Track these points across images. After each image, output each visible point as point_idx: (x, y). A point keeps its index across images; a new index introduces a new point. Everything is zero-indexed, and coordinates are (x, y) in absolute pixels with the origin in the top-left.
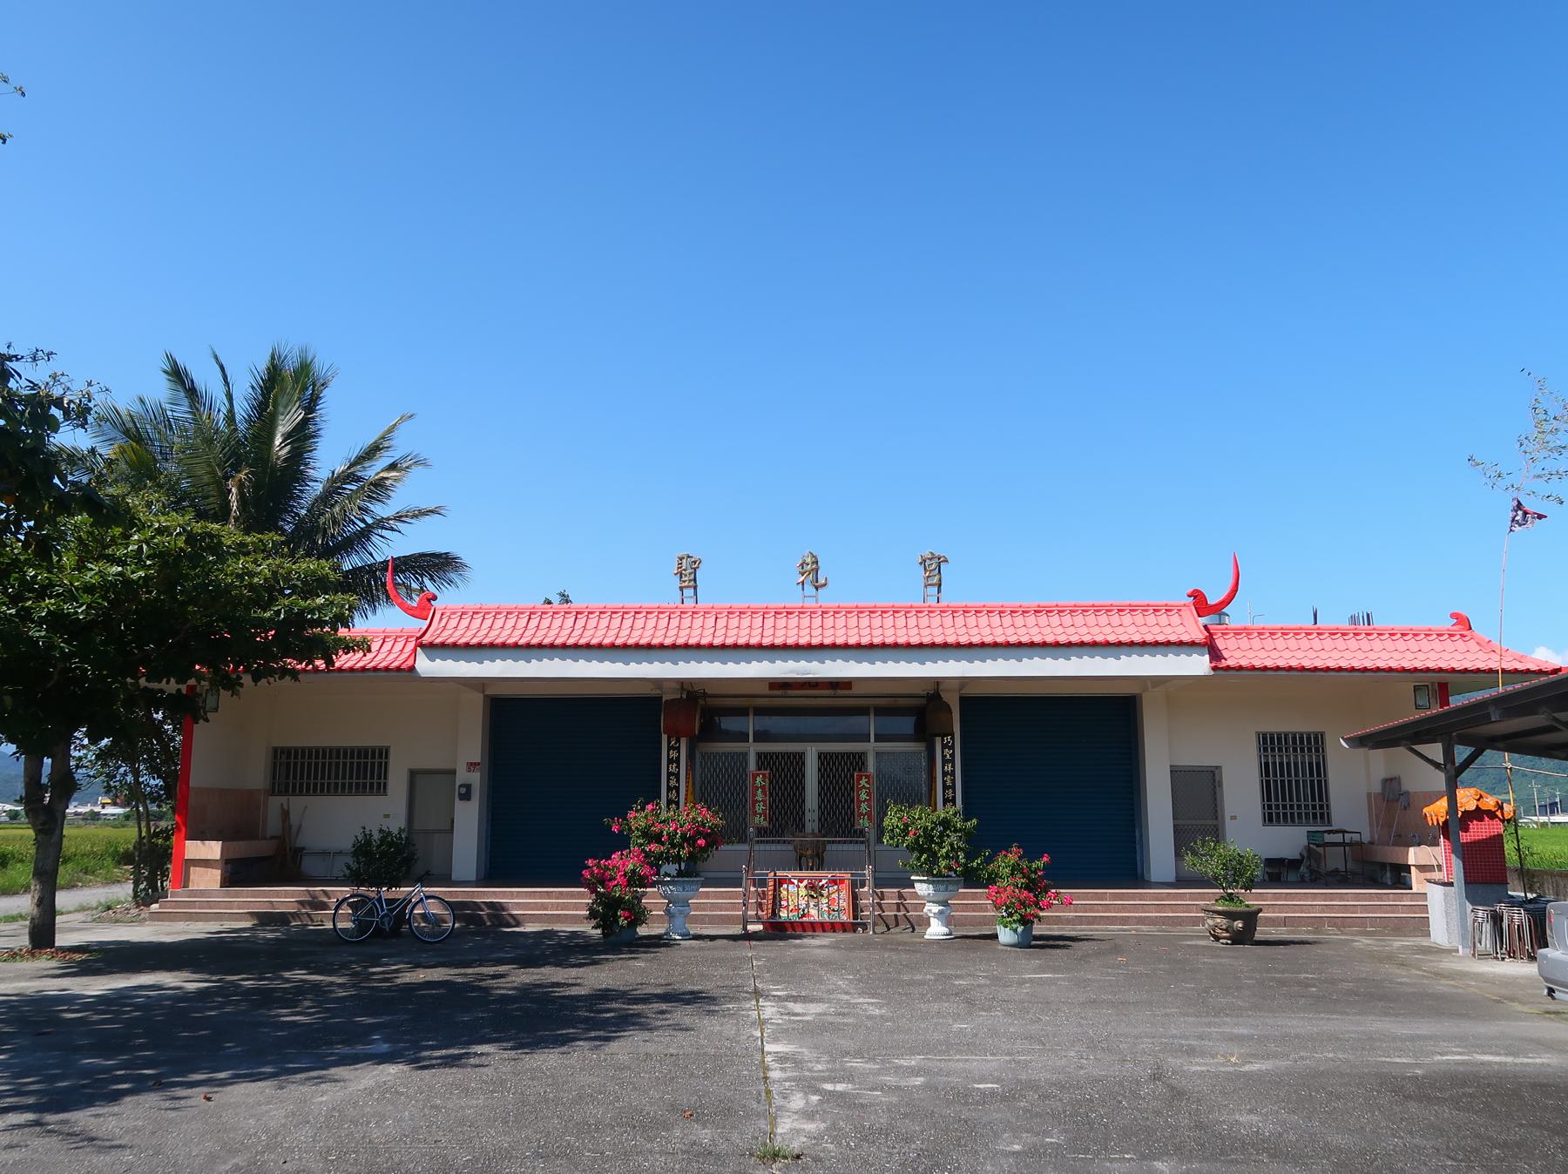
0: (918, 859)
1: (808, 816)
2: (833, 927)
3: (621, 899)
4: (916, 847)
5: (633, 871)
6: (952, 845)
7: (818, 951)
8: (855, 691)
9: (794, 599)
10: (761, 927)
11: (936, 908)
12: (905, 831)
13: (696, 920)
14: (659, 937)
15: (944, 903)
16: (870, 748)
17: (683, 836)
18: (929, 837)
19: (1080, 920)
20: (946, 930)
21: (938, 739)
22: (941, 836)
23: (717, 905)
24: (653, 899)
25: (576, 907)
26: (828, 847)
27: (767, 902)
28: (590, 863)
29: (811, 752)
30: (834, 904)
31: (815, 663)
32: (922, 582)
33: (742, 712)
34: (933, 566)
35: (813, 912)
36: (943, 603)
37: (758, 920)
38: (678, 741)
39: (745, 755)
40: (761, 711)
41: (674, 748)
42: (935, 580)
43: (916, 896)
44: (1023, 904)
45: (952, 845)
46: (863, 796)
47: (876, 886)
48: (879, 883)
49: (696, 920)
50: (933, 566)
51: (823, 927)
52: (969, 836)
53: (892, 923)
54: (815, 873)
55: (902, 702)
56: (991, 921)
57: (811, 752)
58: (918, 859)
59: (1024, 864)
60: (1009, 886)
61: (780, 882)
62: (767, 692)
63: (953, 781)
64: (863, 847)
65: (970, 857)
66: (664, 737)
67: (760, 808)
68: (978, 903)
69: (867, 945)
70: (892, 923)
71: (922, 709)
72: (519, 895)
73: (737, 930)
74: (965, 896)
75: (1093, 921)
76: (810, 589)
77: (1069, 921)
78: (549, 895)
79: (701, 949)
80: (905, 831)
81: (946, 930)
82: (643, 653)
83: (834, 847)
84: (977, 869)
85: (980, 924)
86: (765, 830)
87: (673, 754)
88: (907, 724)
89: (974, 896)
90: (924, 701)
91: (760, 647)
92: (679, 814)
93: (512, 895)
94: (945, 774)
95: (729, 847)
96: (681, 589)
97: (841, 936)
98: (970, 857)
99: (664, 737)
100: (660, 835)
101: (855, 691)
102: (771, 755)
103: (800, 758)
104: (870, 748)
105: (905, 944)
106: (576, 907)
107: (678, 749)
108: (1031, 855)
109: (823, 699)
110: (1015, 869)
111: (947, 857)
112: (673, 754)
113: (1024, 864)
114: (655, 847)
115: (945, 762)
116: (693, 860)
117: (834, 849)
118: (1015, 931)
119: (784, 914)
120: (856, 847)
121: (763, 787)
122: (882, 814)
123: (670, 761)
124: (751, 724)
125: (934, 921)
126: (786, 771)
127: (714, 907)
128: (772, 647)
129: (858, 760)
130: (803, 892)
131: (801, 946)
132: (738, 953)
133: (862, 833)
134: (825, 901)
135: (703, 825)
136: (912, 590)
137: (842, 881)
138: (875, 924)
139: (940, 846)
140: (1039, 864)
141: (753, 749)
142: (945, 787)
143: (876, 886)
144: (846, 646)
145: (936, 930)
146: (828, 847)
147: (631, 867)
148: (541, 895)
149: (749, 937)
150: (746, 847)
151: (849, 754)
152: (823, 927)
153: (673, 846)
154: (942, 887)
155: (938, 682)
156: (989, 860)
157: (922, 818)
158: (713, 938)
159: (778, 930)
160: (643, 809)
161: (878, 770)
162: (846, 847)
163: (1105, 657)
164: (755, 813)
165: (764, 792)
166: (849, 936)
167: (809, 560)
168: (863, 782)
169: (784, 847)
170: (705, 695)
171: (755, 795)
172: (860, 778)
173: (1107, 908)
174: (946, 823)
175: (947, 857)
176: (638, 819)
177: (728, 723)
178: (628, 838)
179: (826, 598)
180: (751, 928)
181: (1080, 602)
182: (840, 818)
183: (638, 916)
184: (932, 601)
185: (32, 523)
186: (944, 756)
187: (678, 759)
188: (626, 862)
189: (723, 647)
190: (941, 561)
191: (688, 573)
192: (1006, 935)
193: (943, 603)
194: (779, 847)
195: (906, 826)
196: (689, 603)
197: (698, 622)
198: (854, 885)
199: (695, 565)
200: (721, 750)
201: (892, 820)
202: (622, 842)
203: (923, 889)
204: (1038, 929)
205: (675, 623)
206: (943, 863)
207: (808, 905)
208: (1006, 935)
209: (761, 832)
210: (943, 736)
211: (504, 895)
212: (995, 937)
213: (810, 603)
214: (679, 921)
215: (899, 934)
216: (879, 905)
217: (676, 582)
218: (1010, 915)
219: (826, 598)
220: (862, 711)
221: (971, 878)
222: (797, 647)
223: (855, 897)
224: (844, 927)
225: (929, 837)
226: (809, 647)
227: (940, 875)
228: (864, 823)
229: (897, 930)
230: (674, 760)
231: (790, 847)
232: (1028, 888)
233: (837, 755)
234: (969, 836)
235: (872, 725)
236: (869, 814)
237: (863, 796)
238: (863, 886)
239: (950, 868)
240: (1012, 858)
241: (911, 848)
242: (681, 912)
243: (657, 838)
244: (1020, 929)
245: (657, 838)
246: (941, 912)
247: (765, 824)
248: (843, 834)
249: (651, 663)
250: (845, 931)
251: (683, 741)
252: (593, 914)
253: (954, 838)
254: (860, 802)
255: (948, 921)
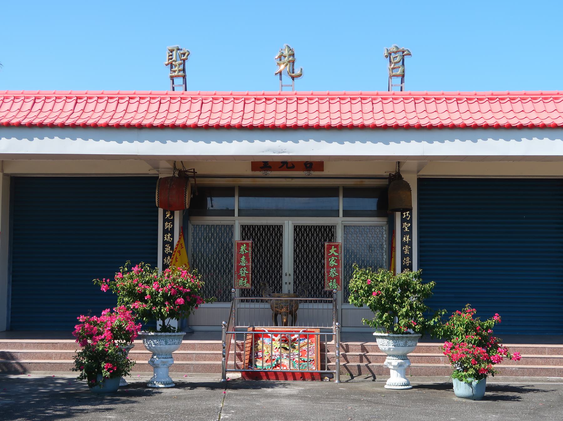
0: (381, 317)
1: (285, 279)
2: (303, 376)
3: (104, 352)
4: (378, 307)
5: (120, 327)
6: (411, 305)
7: (286, 402)
8: (328, 171)
9: (272, 87)
10: (239, 375)
11: (395, 362)
12: (369, 292)
13: (181, 368)
14: (144, 385)
15: (404, 357)
16: (339, 222)
17: (164, 296)
18: (390, 297)
19: (523, 372)
20: (404, 381)
21: (398, 214)
22: (402, 297)
23: (199, 357)
24: (139, 352)
25: (66, 356)
26: (301, 306)
27: (246, 354)
28: (81, 319)
29: (288, 226)
30: (304, 357)
31: (290, 143)
32: (387, 73)
33: (227, 192)
34: (398, 58)
35: (285, 362)
36: (406, 91)
37: (237, 368)
38: (172, 214)
39: (231, 227)
40: (246, 191)
41: (168, 220)
42: (399, 72)
43: (376, 348)
44: (477, 360)
45: (411, 305)
46: (333, 263)
47: (342, 339)
48: (344, 336)
49: (181, 368)
50: (398, 58)
51: (294, 376)
52: (426, 297)
53: (355, 372)
54: (288, 328)
55: (367, 182)
56: (446, 371)
57: (288, 226)
58: (381, 317)
59: (477, 323)
60: (466, 344)
61: (257, 337)
62: (249, 172)
63: (411, 250)
64: (331, 306)
65: (428, 316)
66: (161, 211)
67: (243, 272)
68: (434, 356)
69: (331, 396)
70: (355, 372)
71: (383, 189)
72: (27, 346)
73: (217, 378)
74: (420, 349)
75: (535, 372)
76: (287, 79)
77: (512, 372)
78: (54, 346)
79: (178, 398)
80: (369, 292)
81: (404, 381)
82: (135, 132)
83: (306, 306)
84: (434, 327)
85: (434, 374)
86: (248, 290)
87: (168, 226)
88: (371, 204)
89: (428, 349)
90: (386, 182)
91: (240, 127)
92: (171, 274)
93: (21, 346)
94: (403, 244)
95: (209, 305)
96: (172, 78)
97: (309, 384)
98: (428, 316)
99: (161, 211)
100: (144, 294)
101: (328, 171)
102: (253, 227)
103: (279, 229)
104: (339, 222)
105: (367, 393)
106: (66, 356)
107: (173, 221)
108: (483, 315)
109: (298, 178)
110: (469, 328)
111: (407, 315)
112: (168, 226)
113: (477, 323)
114: (140, 306)
115: (403, 233)
116: (178, 314)
117: (306, 308)
118: (470, 384)
119: (259, 364)
120: (325, 306)
121: (246, 255)
122: (348, 276)
123: (165, 232)
124: (236, 202)
125: (393, 373)
126: (265, 241)
127: (199, 357)
128: (251, 128)
129: (328, 233)
130: (277, 344)
131: (271, 396)
132: (205, 404)
133: (330, 294)
134: (296, 352)
135: (184, 285)
136: (377, 79)
137: (312, 336)
138: (340, 373)
139: (401, 306)
140: (490, 322)
141: (238, 222)
142: (403, 256)
143: (342, 339)
144: (318, 128)
145: (395, 380)
146: (301, 306)
147: (116, 323)
148: (47, 346)
149: (227, 385)
150: (228, 305)
151: (320, 227)
152: (294, 376)
153: (155, 304)
154: (401, 343)
155: (399, 161)
156: (445, 319)
157: (385, 280)
158: (193, 386)
159: (254, 379)
160: (130, 271)
161: (346, 239)
162: (315, 306)
163: (553, 139)
164: (239, 277)
165: (247, 259)
166: (317, 384)
167: (286, 53)
168: (332, 251)
169: (262, 305)
170: (195, 176)
171: (239, 261)
172: (330, 247)
173: (546, 361)
174: (405, 286)
175: (407, 315)
176: (124, 280)
177: (217, 203)
178: (116, 296)
179: (301, 87)
180: (231, 376)
181: (529, 91)
182: (312, 283)
183: (120, 366)
184: (396, 90)
185: (383, 303)
186: (402, 229)
187: (172, 229)
188: (114, 318)
189: (207, 127)
190: (404, 54)
191: (178, 64)
192: (461, 388)
193: (406, 91)
194: (257, 305)
195: (370, 287)
196: (179, 90)
197: (186, 107)
198: (322, 338)
199: (184, 57)
200: (210, 223)
201: (356, 282)
202: (110, 301)
203: (384, 344)
204: (490, 381)
205: (164, 107)
206: (403, 322)
207: (281, 355)
208: (461, 388)
209: (244, 292)
210: (403, 211)
211: (14, 345)
212: (449, 386)
213: (287, 91)
214: (162, 371)
215: (363, 384)
216: (345, 356)
217: (168, 72)
218: (466, 369)
219: (301, 87)
220: (330, 192)
221: (427, 334)
222: (274, 128)
223: (323, 349)
224: (313, 376)
225: (390, 297)
226: (284, 128)
227: (399, 332)
228: (332, 285)
229: (360, 378)
230: (169, 228)
231: (267, 306)
232: (480, 344)
233: (310, 228)
234: (426, 297)
235: (341, 203)
236: (337, 278)
237: (333, 263)
238: (330, 338)
239: (409, 326)
240: (466, 318)
241: (373, 308)
242: (164, 363)
243: (141, 297)
244: (475, 382)
245: (141, 297)
246: (400, 365)
247: (248, 286)
248: (310, 295)
249: (142, 141)
250: (313, 379)
251: (177, 214)
252: (79, 366)
253: (413, 299)
254: (329, 267)
255: (407, 372)
